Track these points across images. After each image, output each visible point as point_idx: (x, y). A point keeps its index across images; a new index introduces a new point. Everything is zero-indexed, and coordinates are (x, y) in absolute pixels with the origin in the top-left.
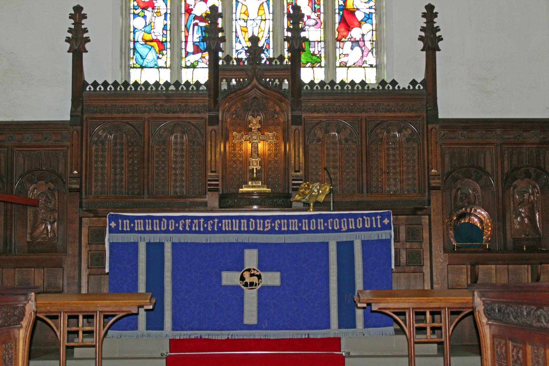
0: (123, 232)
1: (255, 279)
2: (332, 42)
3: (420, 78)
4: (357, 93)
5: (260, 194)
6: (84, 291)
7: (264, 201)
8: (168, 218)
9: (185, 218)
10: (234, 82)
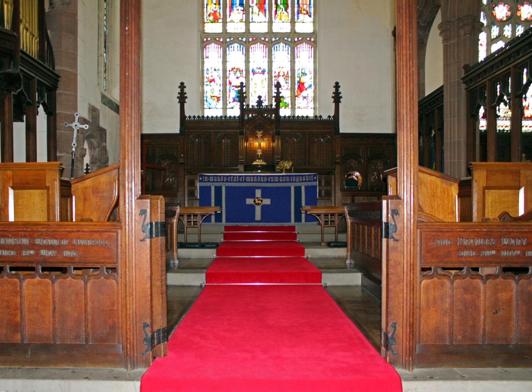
0: (205, 182)
1: (260, 202)
2: (293, 98)
3: (332, 114)
4: (304, 121)
5: (261, 165)
6: (186, 206)
7: (264, 168)
8: (224, 176)
9: (231, 176)
10: (250, 115)
